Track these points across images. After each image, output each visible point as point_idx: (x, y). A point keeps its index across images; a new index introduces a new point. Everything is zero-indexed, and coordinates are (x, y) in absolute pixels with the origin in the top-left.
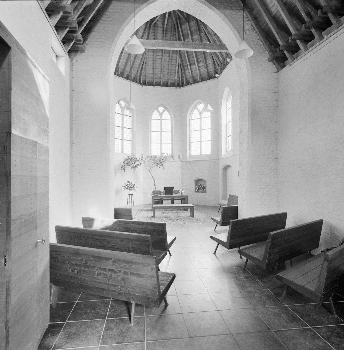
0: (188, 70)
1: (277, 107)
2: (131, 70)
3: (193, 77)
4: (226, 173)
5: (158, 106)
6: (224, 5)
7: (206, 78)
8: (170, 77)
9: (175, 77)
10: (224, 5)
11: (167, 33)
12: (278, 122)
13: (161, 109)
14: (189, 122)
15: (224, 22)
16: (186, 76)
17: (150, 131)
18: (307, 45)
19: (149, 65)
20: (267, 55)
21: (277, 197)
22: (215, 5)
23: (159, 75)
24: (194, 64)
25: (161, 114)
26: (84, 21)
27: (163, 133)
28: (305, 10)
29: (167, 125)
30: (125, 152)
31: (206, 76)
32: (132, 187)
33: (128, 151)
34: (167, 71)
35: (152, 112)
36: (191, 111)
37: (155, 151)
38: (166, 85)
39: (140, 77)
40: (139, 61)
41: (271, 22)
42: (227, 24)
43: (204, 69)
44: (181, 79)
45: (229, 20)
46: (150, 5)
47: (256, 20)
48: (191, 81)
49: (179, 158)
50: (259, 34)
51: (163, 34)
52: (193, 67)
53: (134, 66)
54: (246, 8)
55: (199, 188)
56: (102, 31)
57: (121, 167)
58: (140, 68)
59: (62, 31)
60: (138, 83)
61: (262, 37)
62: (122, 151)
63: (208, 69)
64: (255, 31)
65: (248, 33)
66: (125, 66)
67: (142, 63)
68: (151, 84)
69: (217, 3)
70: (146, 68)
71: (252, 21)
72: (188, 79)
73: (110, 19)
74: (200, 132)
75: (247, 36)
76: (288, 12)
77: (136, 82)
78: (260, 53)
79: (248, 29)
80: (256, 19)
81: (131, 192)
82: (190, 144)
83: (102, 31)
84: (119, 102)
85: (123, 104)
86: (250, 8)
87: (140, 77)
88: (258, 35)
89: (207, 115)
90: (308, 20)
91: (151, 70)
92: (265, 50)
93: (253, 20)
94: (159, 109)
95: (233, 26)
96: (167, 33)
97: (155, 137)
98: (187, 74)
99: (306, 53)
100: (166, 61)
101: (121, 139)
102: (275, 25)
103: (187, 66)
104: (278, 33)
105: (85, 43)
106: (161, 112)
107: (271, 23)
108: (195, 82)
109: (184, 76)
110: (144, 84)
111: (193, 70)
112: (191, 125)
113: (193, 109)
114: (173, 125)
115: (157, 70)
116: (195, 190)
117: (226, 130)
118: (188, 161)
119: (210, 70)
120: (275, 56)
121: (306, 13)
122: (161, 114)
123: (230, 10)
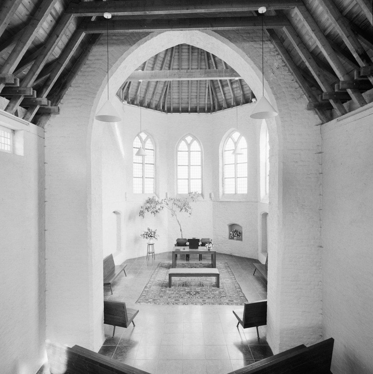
0: (220, 92)
1: (322, 173)
2: (153, 96)
3: (226, 100)
4: (266, 219)
5: (185, 136)
6: (243, 36)
7: (242, 101)
8: (199, 101)
9: (205, 101)
10: (243, 37)
11: (193, 51)
12: (322, 195)
13: (189, 139)
14: (222, 154)
15: (243, 60)
16: (218, 99)
17: (176, 166)
18: (363, 94)
19: (174, 88)
20: (305, 100)
21: (321, 301)
22: (229, 37)
23: (186, 100)
24: (227, 85)
25: (189, 145)
26: (50, 80)
27: (191, 167)
28: (359, 50)
29: (197, 158)
30: (145, 192)
31: (241, 99)
32: (152, 235)
33: (150, 190)
34: (195, 94)
35: (179, 143)
36: (224, 141)
37: (182, 189)
38: (194, 110)
39: (164, 103)
40: (162, 86)
41: (308, 59)
42: (247, 62)
43: (239, 91)
44: (212, 103)
45: (250, 57)
46: (141, 46)
47: (289, 54)
48: (224, 105)
49: (210, 197)
50: (294, 74)
51: (189, 52)
52: (226, 89)
53: (156, 92)
54: (274, 39)
55: (233, 235)
56: (81, 85)
57: (139, 213)
58: (164, 94)
59: (14, 102)
60: (161, 111)
61: (297, 77)
62: (143, 192)
63: (243, 92)
64: (287, 69)
65: (277, 72)
66: (146, 93)
67: (166, 87)
68: (176, 110)
69: (233, 35)
70: (170, 92)
71: (282, 56)
72: (221, 103)
73: (90, 69)
74: (235, 165)
75: (276, 76)
76: (333, 48)
77: (160, 110)
78: (296, 100)
79: (277, 66)
80: (288, 53)
81: (152, 241)
82: (223, 181)
83: (81, 85)
84: (138, 135)
85: (144, 136)
86: (280, 38)
87: (164, 103)
88: (292, 74)
89: (243, 143)
90: (364, 66)
91: (177, 94)
92: (303, 93)
93: (284, 54)
94: (186, 139)
95: (255, 64)
96: (193, 51)
97: (182, 172)
98: (219, 97)
99: (361, 108)
100: (193, 83)
101: (142, 177)
102: (314, 64)
103: (219, 87)
104: (319, 76)
105: (60, 102)
106: (189, 142)
107: (308, 62)
108: (229, 106)
109: (216, 100)
110: (169, 111)
111: (226, 92)
112: (224, 158)
113: (226, 139)
114: (203, 158)
115: (183, 94)
116: (229, 237)
117: (266, 166)
118: (221, 201)
119: (246, 93)
120: (317, 103)
121: (361, 54)
122: (189, 145)
123: (251, 43)
